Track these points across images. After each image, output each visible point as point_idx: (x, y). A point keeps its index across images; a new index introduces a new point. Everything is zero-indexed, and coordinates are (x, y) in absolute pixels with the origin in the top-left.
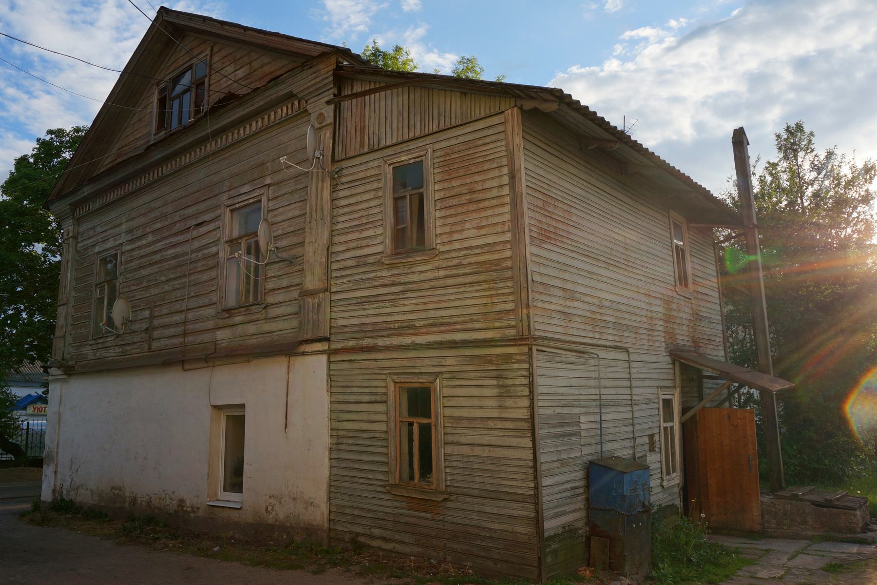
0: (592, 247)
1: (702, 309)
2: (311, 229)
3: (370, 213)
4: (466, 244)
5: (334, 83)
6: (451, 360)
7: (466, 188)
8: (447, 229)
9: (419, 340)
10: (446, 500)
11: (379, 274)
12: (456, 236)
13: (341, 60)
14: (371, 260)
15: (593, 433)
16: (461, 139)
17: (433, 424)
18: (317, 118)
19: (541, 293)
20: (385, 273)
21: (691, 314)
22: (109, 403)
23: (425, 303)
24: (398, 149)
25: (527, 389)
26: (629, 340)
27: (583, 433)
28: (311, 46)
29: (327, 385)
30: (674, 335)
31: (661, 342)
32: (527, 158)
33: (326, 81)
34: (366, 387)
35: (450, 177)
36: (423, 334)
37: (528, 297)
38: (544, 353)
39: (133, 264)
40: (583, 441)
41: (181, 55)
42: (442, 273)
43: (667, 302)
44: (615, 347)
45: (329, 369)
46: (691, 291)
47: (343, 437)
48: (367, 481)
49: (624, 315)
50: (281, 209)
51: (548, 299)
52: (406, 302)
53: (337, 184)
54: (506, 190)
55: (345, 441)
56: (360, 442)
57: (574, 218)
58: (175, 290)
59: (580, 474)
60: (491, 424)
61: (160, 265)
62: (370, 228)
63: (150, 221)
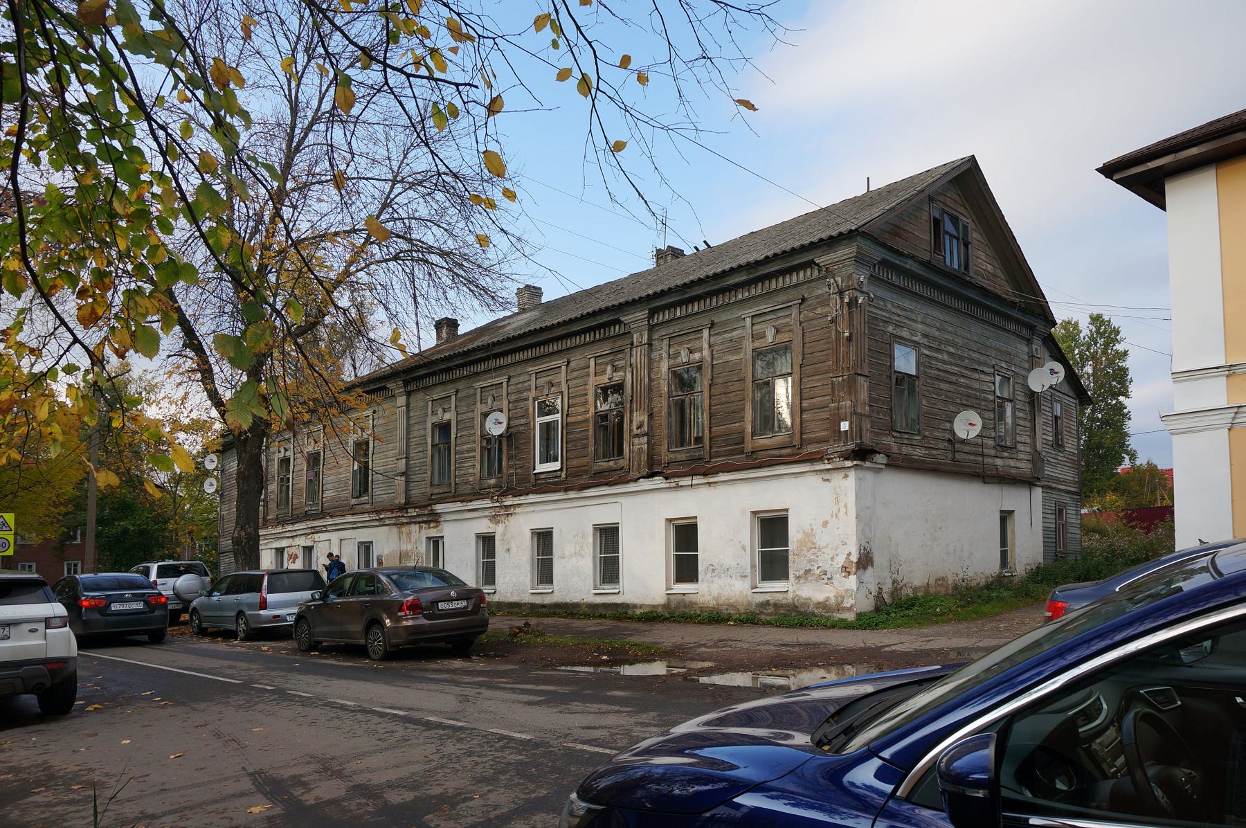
9: (1060, 487)
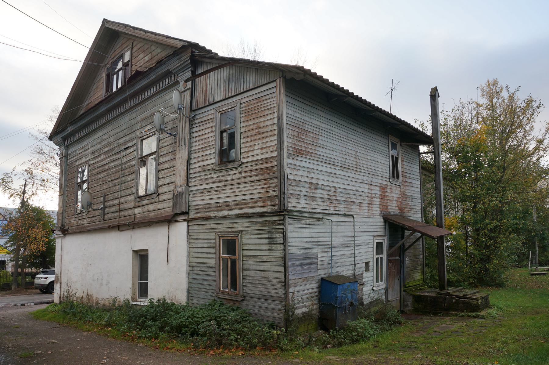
0: (331, 158)
1: (408, 191)
2: (179, 150)
3: (209, 141)
4: (255, 158)
5: (191, 64)
6: (246, 225)
7: (256, 125)
8: (246, 150)
10: (243, 300)
11: (212, 176)
12: (251, 154)
13: (194, 50)
14: (209, 167)
15: (326, 262)
16: (255, 97)
17: (237, 259)
18: (183, 85)
19: (293, 186)
20: (215, 175)
21: (399, 194)
22: (85, 249)
23: (235, 192)
24: (223, 103)
25: (282, 240)
26: (355, 210)
27: (319, 263)
28: (178, 42)
29: (187, 238)
30: (387, 207)
31: (377, 210)
32: (288, 107)
33: (187, 63)
34: (206, 239)
35: (248, 119)
36: (234, 209)
37: (284, 188)
38: (293, 220)
39: (95, 171)
40: (319, 267)
41: (117, 48)
42: (243, 175)
43: (383, 188)
44: (345, 215)
45: (188, 230)
46: (401, 181)
47: (195, 266)
48: (206, 290)
49: (352, 196)
50: (166, 139)
51: (298, 189)
52: (225, 192)
53: (193, 124)
54: (275, 127)
55: (196, 269)
56: (203, 269)
57: (320, 142)
58: (115, 186)
59: (316, 285)
60: (265, 259)
61: (107, 172)
62: (209, 149)
63: (102, 146)
